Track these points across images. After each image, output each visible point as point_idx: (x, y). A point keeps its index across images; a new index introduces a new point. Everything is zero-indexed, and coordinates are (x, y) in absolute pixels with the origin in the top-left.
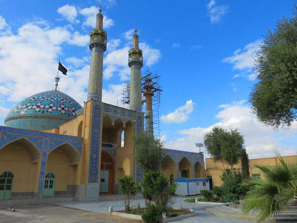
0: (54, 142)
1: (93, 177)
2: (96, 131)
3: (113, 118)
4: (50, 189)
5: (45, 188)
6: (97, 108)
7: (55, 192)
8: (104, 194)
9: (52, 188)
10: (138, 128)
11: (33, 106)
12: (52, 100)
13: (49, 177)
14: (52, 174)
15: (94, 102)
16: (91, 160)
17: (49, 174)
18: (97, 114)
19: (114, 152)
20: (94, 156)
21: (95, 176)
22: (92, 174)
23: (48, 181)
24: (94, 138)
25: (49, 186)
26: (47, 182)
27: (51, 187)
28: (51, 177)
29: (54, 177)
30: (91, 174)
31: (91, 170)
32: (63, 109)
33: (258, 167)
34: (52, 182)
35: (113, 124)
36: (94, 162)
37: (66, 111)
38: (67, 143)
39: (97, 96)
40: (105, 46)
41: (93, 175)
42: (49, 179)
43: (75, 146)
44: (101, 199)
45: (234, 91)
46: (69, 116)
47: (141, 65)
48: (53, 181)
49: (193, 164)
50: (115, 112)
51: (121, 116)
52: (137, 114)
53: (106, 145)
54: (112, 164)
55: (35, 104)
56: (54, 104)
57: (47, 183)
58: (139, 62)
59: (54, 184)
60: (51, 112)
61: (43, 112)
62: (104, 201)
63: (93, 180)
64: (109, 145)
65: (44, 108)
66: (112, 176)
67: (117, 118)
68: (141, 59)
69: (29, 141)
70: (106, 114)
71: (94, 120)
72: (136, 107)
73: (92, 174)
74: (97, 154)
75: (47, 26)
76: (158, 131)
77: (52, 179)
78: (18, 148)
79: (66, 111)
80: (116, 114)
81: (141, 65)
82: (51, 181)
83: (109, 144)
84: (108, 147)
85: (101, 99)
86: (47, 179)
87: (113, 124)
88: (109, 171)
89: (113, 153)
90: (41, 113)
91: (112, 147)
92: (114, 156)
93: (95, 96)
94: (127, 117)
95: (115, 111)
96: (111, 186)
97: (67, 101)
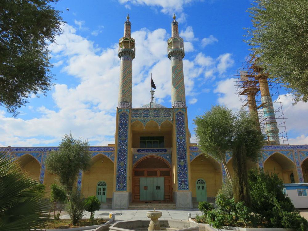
0: (40, 156)
1: (183, 184)
2: (123, 138)
3: (144, 122)
4: (99, 196)
5: (99, 195)
6: (180, 114)
7: (107, 199)
8: (160, 202)
9: (105, 195)
10: (177, 127)
13: (101, 185)
14: (103, 183)
15: (119, 110)
16: (118, 168)
17: (101, 183)
18: (180, 120)
19: (170, 157)
20: (122, 164)
21: (123, 183)
22: (120, 182)
23: (101, 188)
24: (180, 146)
25: (102, 193)
26: (100, 189)
27: (104, 194)
28: (103, 185)
29: (105, 185)
30: (118, 182)
31: (118, 178)
34: (104, 189)
35: (160, 127)
36: (121, 170)
38: (100, 153)
40: (183, 52)
41: (183, 182)
42: (101, 187)
43: (108, 156)
44: (130, 207)
47: (182, 55)
48: (105, 188)
49: (298, 163)
50: (146, 115)
51: (155, 118)
52: (176, 111)
53: (159, 150)
54: (168, 169)
57: (101, 191)
58: (175, 51)
59: (106, 191)
62: (134, 209)
63: (183, 188)
64: (163, 150)
66: (169, 182)
68: (133, 49)
69: (282, 154)
70: (165, 119)
71: (120, 128)
72: (178, 103)
73: (120, 182)
74: (185, 161)
76: (282, 121)
77: (104, 187)
78: (202, 161)
80: (148, 116)
81: (182, 55)
82: (103, 188)
83: (162, 148)
84: (162, 152)
85: (131, 106)
86: (100, 187)
87: (160, 127)
88: (165, 178)
89: (168, 158)
91: (167, 152)
92: (170, 161)
94: (163, 118)
95: (147, 114)
96: (170, 194)
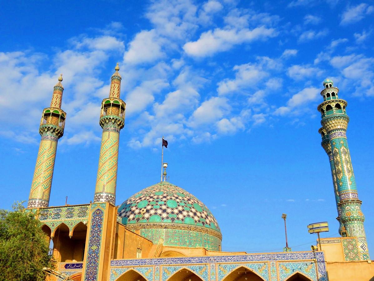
11: (127, 212)
12: (151, 200)
32: (164, 211)
33: (164, 37)
37: (168, 213)
39: (43, 202)
45: (273, 127)
46: (138, 222)
51: (66, 219)
55: (158, 207)
56: (152, 206)
60: (148, 219)
61: (138, 220)
65: (140, 213)
67: (59, 224)
75: (337, 117)
79: (168, 213)
90: (169, 221)
93: (43, 202)
97: (138, 201)
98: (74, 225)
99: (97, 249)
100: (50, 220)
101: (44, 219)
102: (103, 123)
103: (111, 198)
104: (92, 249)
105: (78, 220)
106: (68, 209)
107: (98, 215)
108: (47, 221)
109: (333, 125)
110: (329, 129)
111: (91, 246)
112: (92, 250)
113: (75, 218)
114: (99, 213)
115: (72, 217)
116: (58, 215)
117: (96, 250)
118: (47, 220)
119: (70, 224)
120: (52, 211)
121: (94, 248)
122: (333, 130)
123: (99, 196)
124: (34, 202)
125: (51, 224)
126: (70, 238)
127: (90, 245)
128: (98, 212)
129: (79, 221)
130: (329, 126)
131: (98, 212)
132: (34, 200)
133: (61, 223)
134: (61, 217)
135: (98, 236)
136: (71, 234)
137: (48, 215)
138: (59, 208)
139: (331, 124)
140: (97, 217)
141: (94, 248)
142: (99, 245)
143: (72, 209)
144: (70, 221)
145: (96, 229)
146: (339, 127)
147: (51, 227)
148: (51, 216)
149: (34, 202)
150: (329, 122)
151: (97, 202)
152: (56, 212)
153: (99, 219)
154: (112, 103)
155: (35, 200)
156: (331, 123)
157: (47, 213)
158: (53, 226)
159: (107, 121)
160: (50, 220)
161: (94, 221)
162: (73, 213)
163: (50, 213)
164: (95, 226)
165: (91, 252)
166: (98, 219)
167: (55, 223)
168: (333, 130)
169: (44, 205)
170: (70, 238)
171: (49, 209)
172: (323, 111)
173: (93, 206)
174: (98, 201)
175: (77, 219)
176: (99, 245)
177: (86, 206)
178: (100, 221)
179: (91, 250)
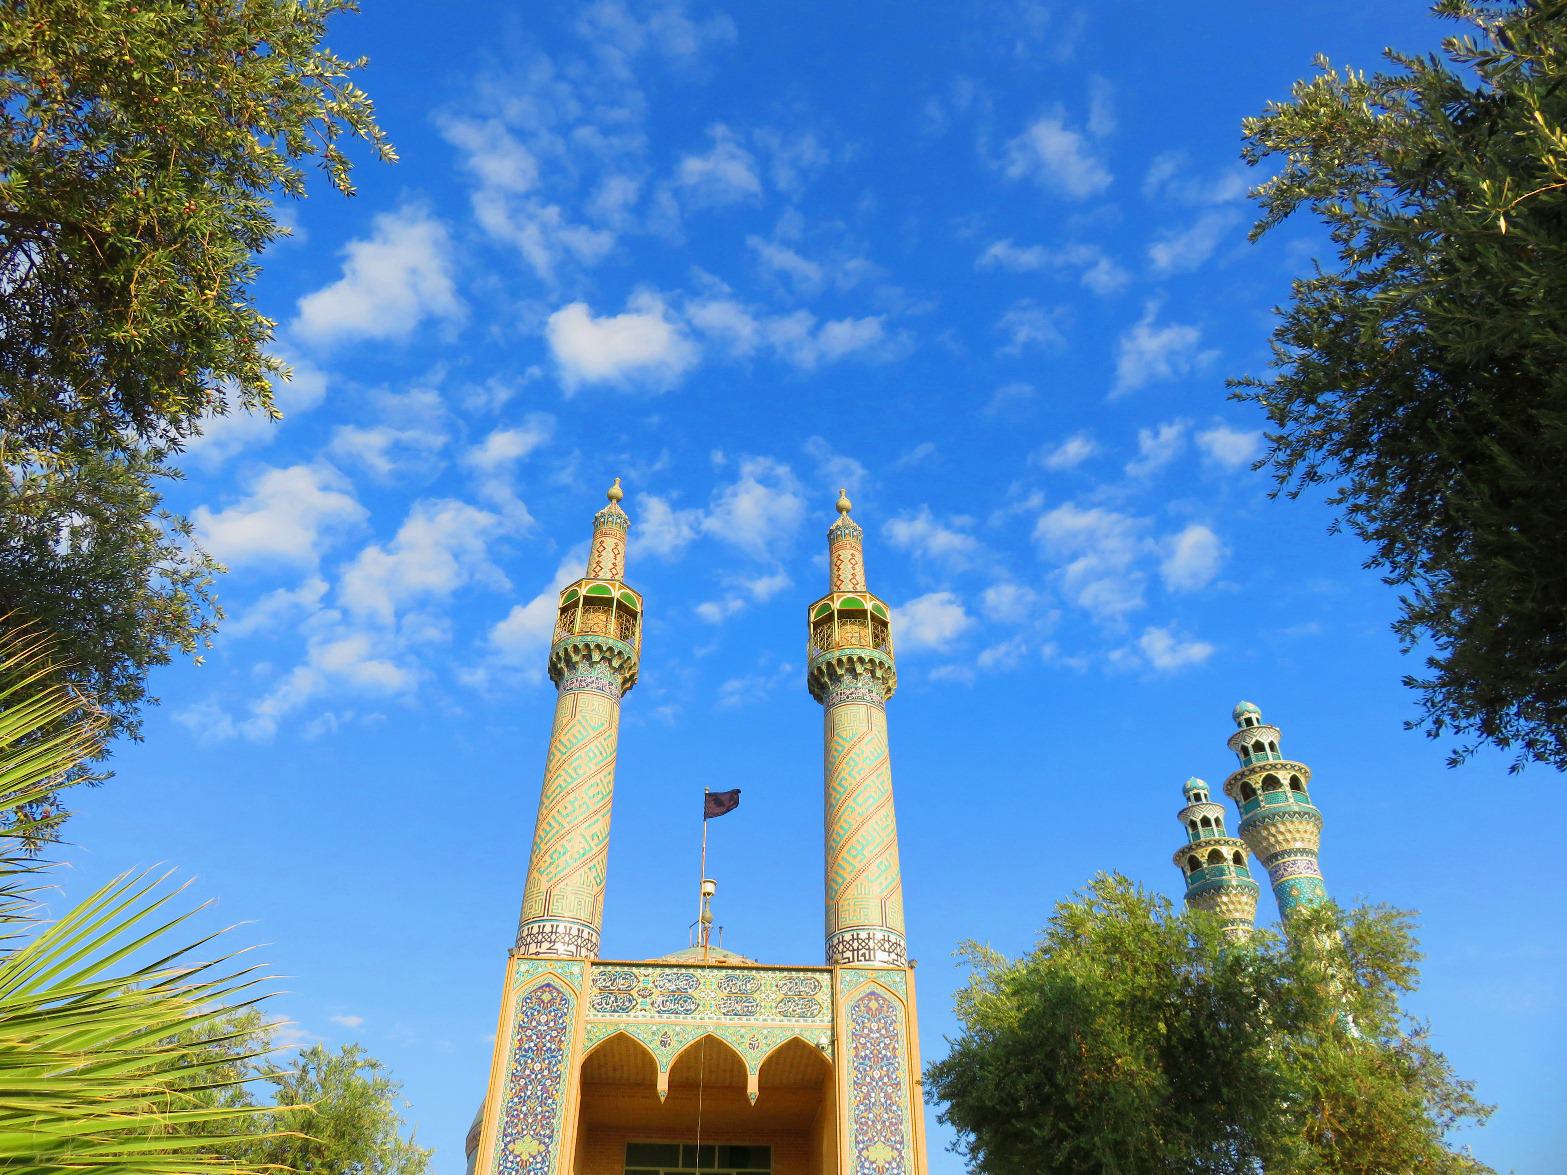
39: (585, 935)
51: (726, 1020)
67: (691, 1037)
98: (766, 1050)
99: (894, 1159)
100: (644, 1016)
101: (614, 1011)
102: (575, 658)
103: (579, 941)
104: (872, 1159)
105: (605, 1024)
106: (729, 979)
107: (873, 1015)
108: (631, 1019)
109: (1289, 836)
110: (1273, 846)
111: (863, 1145)
112: (516, 1157)
113: (765, 1020)
114: (880, 1009)
115: (752, 1013)
116: (680, 1000)
117: (890, 1163)
118: (632, 1014)
119: (747, 1041)
120: (650, 979)
121: (526, 1147)
122: (1289, 852)
123: (853, 939)
124: (548, 929)
125: (654, 1034)
126: (753, 1103)
127: (857, 1142)
128: (874, 1005)
129: (788, 1036)
130: (1274, 836)
131: (546, 997)
132: (536, 926)
133: (700, 1034)
134: (700, 1008)
135: (546, 1097)
136: (662, 1085)
137: (632, 992)
138: (683, 971)
139: (1282, 833)
140: (543, 1019)
141: (526, 1147)
142: (901, 1143)
143: (747, 980)
144: (743, 1031)
145: (537, 1067)
146: (1298, 845)
147: (653, 1047)
148: (648, 1000)
149: (548, 929)
150: (1274, 825)
151: (863, 964)
152: (673, 988)
153: (552, 1024)
154: (585, 597)
155: (555, 924)
156: (1282, 828)
157: (630, 988)
158: (664, 1044)
159: (596, 657)
160: (644, 1016)
161: (863, 1040)
162: (755, 995)
163: (641, 985)
164: (867, 1062)
165: (509, 1165)
166: (878, 1031)
167: (670, 1033)
168: (1289, 852)
169: (579, 941)
170: (753, 1103)
171: (634, 970)
172: (1248, 792)
173: (848, 979)
174: (869, 960)
175: (777, 1023)
176: (901, 1143)
177: (810, 974)
178: (554, 1034)
179: (511, 1158)
